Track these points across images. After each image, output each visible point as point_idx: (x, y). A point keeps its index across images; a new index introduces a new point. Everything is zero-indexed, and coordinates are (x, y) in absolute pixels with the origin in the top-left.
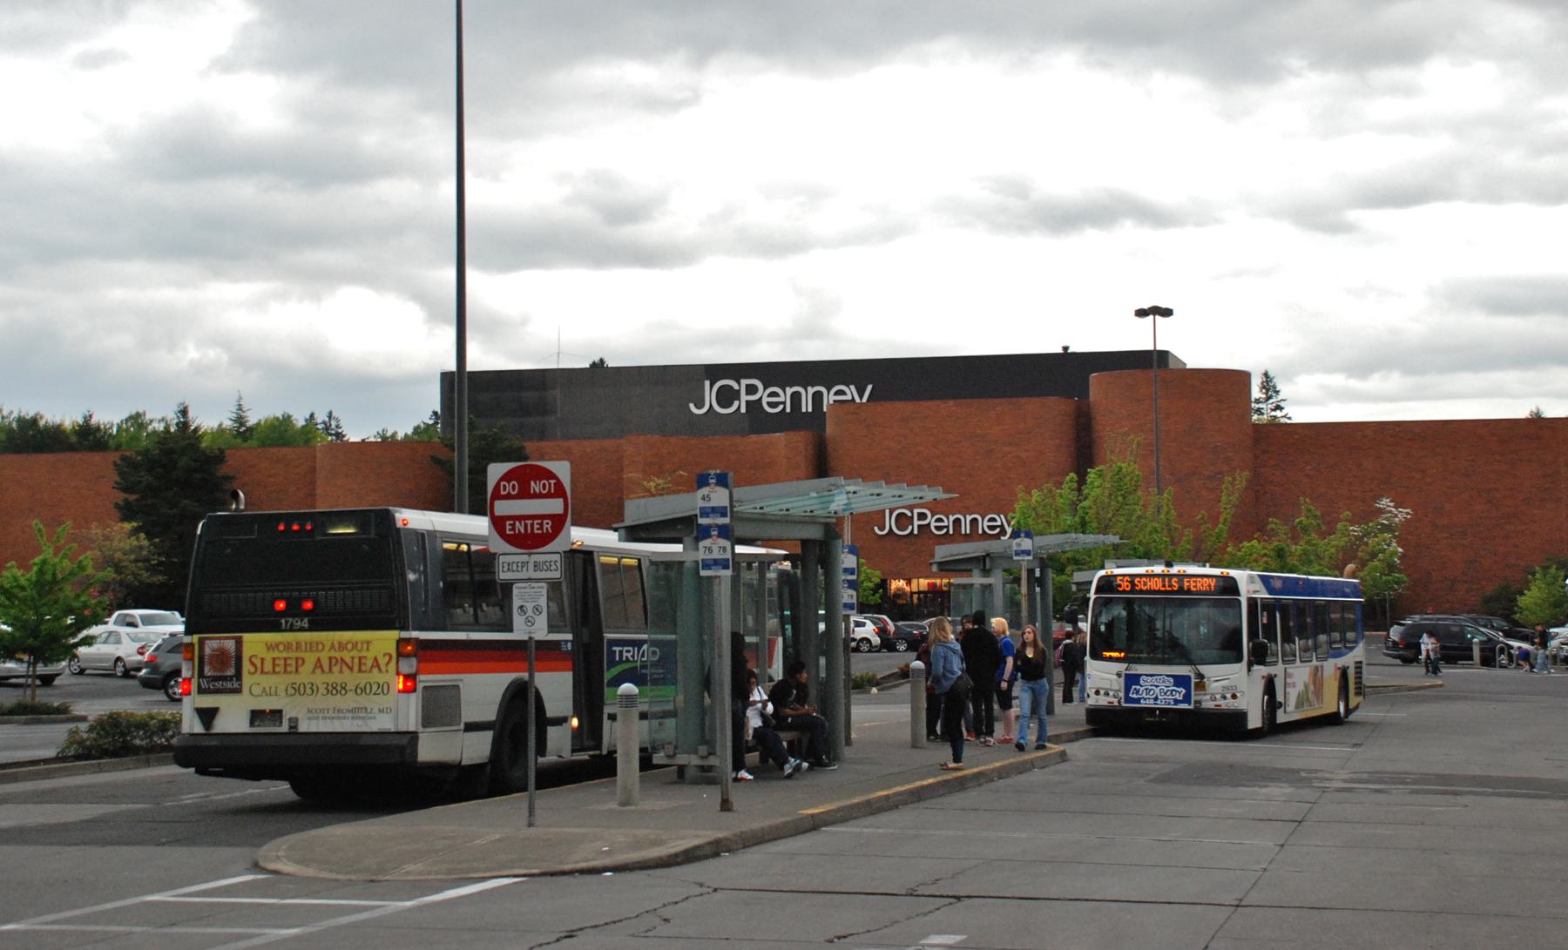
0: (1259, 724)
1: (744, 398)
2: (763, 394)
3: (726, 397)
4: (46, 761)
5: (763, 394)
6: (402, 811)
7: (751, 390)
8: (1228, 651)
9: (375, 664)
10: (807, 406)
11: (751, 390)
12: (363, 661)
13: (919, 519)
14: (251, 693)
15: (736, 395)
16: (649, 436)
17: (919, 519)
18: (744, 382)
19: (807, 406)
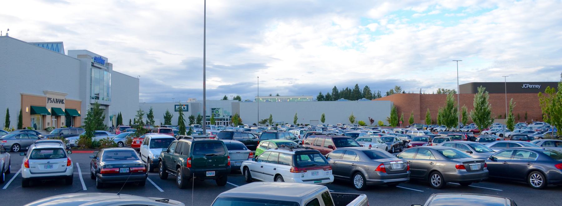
0: (302, 159)
1: (527, 86)
2: (529, 86)
3: (526, 86)
4: (91, 74)
5: (529, 86)
6: (242, 185)
7: (528, 85)
8: (428, 93)
9: (484, 151)
10: (534, 87)
11: (528, 85)
12: (551, 134)
13: (208, 122)
14: (68, 154)
15: (526, 86)
16: (474, 102)
17: (208, 122)
18: (527, 85)
19: (534, 87)
